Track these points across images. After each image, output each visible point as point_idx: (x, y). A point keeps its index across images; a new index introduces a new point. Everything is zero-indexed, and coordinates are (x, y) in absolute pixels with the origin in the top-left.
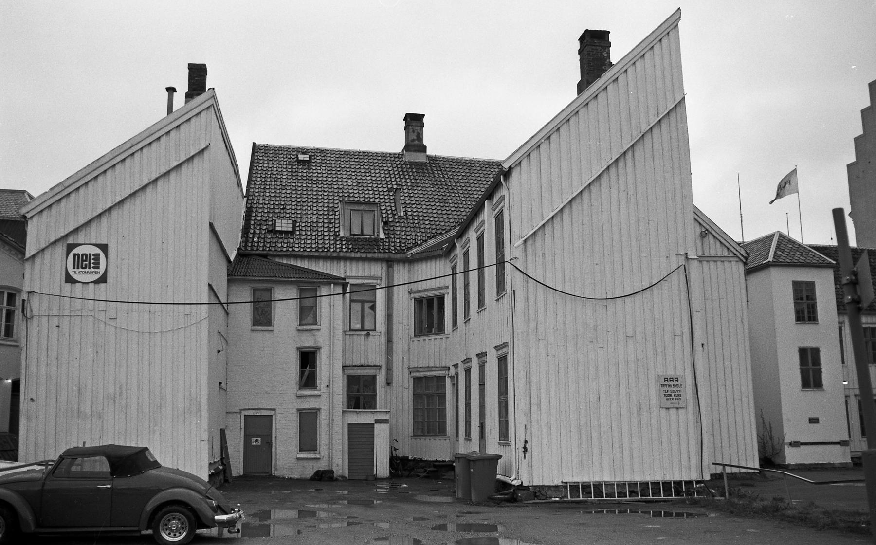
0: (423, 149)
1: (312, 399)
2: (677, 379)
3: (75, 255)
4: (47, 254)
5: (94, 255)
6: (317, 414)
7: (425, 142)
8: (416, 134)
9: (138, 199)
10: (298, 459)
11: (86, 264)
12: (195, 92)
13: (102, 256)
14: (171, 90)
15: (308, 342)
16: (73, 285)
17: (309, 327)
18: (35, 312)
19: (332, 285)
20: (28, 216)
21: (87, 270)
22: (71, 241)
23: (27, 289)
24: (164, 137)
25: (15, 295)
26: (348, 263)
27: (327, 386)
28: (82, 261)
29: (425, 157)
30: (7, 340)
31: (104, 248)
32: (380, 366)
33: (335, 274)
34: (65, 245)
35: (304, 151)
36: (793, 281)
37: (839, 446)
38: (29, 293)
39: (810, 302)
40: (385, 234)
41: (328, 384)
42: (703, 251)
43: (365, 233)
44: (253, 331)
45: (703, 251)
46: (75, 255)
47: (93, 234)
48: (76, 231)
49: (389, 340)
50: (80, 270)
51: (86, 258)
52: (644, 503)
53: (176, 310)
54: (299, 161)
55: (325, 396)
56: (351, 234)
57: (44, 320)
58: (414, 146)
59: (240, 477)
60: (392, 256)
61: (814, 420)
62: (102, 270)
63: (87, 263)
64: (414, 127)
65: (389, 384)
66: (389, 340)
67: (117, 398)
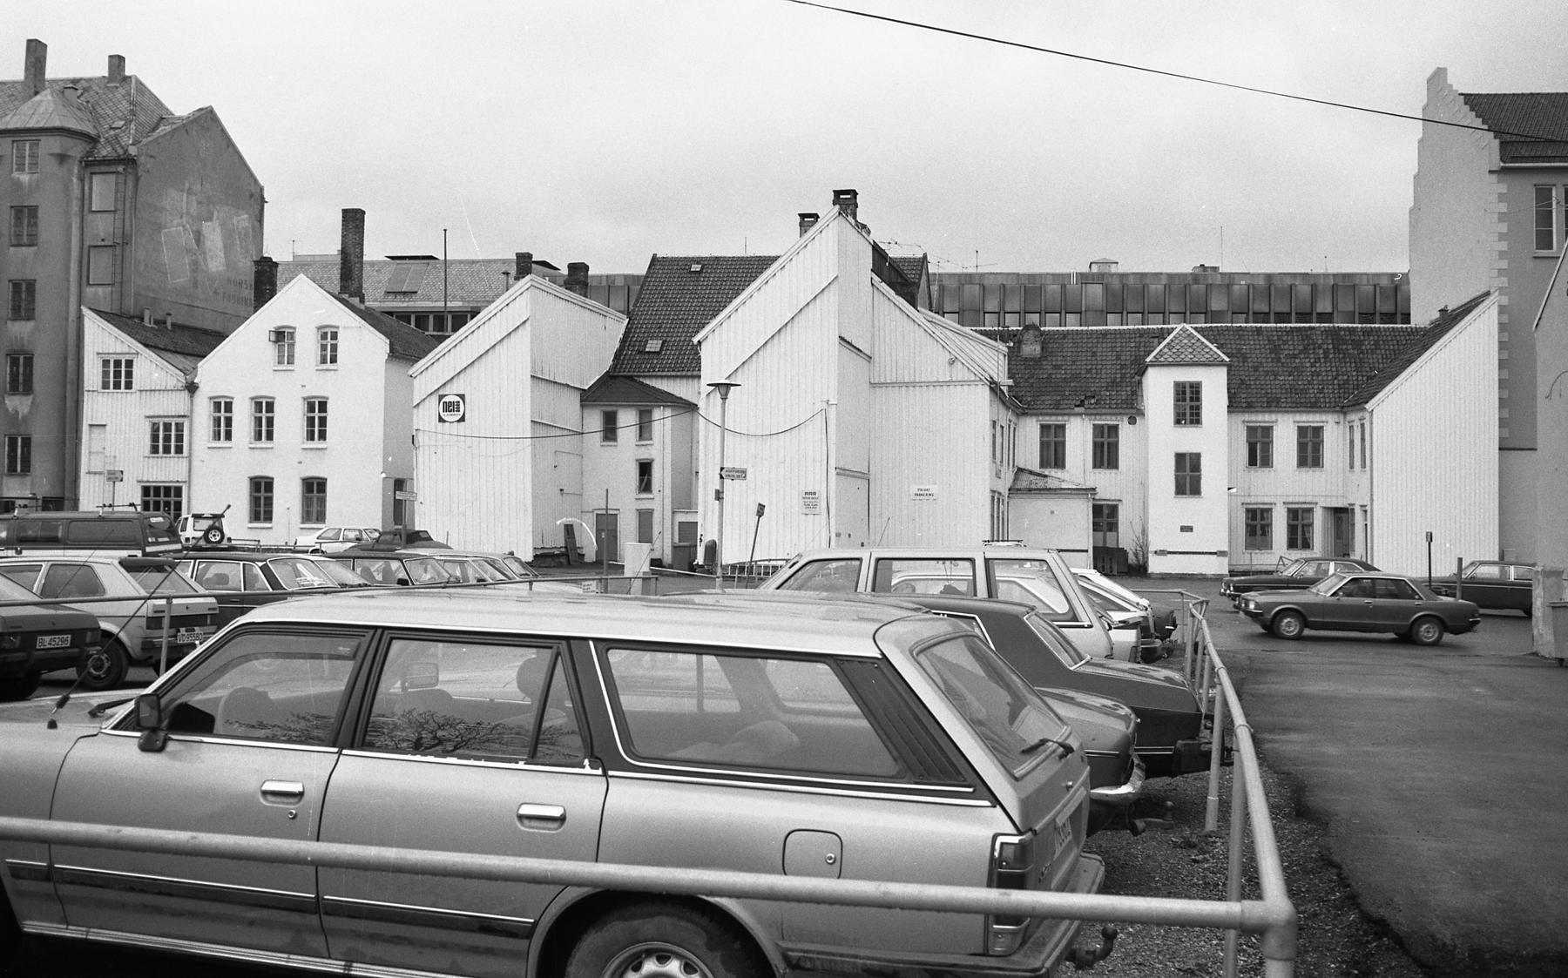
2: (815, 493)
9: (483, 359)
15: (644, 455)
18: (421, 444)
22: (441, 393)
23: (415, 428)
28: (449, 407)
31: (462, 397)
35: (698, 260)
37: (1215, 556)
38: (417, 430)
39: (1194, 404)
44: (602, 446)
47: (455, 388)
54: (691, 272)
57: (427, 448)
59: (593, 562)
61: (1187, 529)
62: (461, 413)
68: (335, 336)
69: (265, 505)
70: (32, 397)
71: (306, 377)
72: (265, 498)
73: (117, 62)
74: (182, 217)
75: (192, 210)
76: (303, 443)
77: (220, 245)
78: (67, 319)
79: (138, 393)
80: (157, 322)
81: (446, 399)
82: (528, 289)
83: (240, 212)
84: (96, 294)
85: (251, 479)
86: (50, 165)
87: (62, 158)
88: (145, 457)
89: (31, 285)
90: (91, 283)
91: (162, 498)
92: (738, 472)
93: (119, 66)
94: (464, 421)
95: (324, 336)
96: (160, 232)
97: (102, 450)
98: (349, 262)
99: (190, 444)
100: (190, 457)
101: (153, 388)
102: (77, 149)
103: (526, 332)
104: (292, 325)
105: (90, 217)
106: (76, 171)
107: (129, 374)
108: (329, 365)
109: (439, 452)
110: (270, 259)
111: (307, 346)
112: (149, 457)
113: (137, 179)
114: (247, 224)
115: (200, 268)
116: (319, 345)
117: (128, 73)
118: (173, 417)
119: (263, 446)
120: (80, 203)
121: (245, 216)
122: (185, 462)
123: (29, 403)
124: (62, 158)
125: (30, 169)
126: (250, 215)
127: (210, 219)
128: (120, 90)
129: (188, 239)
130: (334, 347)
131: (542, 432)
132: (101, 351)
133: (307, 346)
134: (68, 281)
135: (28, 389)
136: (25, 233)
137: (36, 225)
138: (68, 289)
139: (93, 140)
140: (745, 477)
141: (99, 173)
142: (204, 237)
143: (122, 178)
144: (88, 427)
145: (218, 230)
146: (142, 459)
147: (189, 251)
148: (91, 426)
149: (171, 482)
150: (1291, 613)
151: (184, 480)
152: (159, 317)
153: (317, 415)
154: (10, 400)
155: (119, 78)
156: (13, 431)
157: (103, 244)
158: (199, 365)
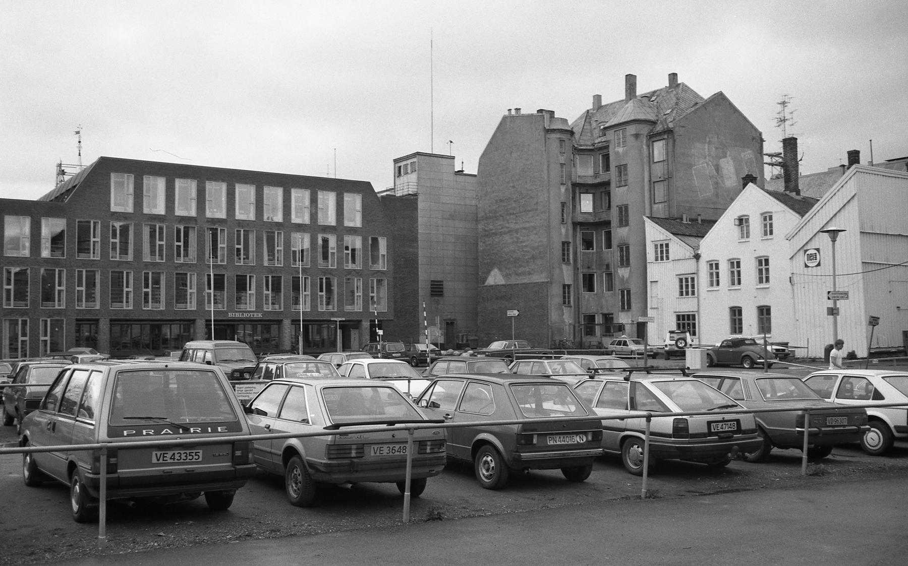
13: (818, 254)
18: (796, 282)
22: (805, 249)
28: (811, 257)
31: (818, 250)
36: (828, 308)
42: (314, 200)
45: (314, 200)
48: (807, 243)
52: (618, 420)
57: (799, 285)
62: (818, 261)
71: (756, 245)
73: (673, 77)
74: (705, 158)
75: (712, 153)
76: (757, 285)
80: (691, 220)
81: (808, 252)
82: (854, 174)
84: (658, 208)
86: (631, 141)
87: (637, 136)
89: (626, 207)
91: (686, 322)
92: (841, 294)
93: (674, 79)
95: (765, 219)
98: (788, 171)
99: (698, 289)
100: (698, 297)
102: (645, 130)
103: (855, 202)
104: (770, 211)
105: (653, 166)
106: (645, 142)
108: (769, 237)
109: (806, 287)
110: (752, 175)
111: (756, 225)
113: (674, 141)
114: (751, 156)
117: (679, 82)
118: (688, 274)
119: (736, 288)
120: (648, 159)
121: (749, 152)
123: (628, 271)
124: (637, 136)
125: (623, 144)
127: (725, 157)
128: (674, 92)
130: (771, 225)
131: (870, 268)
133: (756, 225)
135: (628, 264)
138: (644, 207)
139: (654, 123)
140: (847, 297)
141: (658, 141)
145: (731, 162)
148: (651, 282)
149: (689, 312)
152: (693, 217)
153: (764, 267)
154: (620, 271)
155: (675, 85)
156: (623, 287)
157: (660, 179)
158: (701, 243)
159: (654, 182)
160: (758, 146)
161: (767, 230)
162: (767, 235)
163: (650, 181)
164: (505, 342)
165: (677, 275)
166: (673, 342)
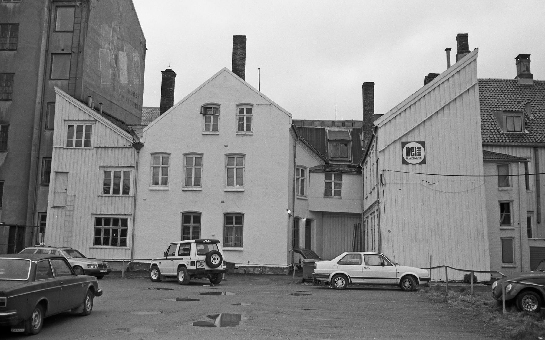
0: (531, 76)
1: (510, 231)
3: (407, 148)
4: (391, 148)
5: (418, 148)
6: (512, 241)
7: (532, 72)
8: (525, 67)
10: (503, 267)
11: (413, 154)
12: (464, 51)
13: (422, 149)
14: (448, 50)
15: (505, 197)
16: (407, 165)
17: (504, 188)
18: (387, 182)
19: (519, 163)
20: (379, 126)
21: (414, 157)
22: (404, 140)
24: (451, 78)
25: (304, 170)
26: (510, 149)
27: (519, 224)
28: (411, 152)
29: (532, 82)
30: (302, 196)
31: (423, 144)
32: (533, 212)
33: (518, 156)
34: (401, 143)
40: (528, 130)
41: (519, 223)
43: (516, 130)
46: (407, 148)
49: (538, 196)
50: (411, 157)
51: (413, 150)
53: (452, 179)
55: (517, 230)
56: (507, 131)
58: (525, 75)
60: (537, 144)
62: (423, 157)
63: (414, 153)
64: (524, 63)
65: (539, 222)
66: (538, 196)
67: (437, 230)
68: (249, 111)
69: (193, 233)
70: (6, 154)
72: (194, 228)
76: (150, 186)
77: (126, 67)
78: (35, 101)
79: (95, 150)
83: (136, 51)
85: (183, 213)
88: (98, 196)
90: (52, 78)
94: (425, 163)
96: (98, 49)
97: (65, 191)
101: (107, 146)
104: (218, 103)
106: (47, 3)
107: (88, 136)
108: (245, 132)
112: (102, 196)
113: (89, 11)
115: (116, 79)
116: (238, 118)
121: (137, 54)
122: (130, 201)
123: (4, 158)
126: (140, 53)
129: (111, 59)
132: (67, 119)
134: (37, 75)
136: (8, 42)
137: (16, 36)
142: (119, 61)
143: (78, 10)
144: (54, 173)
146: (96, 197)
147: (112, 66)
148: (57, 173)
150: (340, 275)
151: (130, 214)
157: (62, 52)
159: (52, 54)
160: (143, 51)
161: (243, 125)
162: (242, 130)
163: (47, 51)
164: (76, 312)
165: (101, 167)
166: (203, 258)
